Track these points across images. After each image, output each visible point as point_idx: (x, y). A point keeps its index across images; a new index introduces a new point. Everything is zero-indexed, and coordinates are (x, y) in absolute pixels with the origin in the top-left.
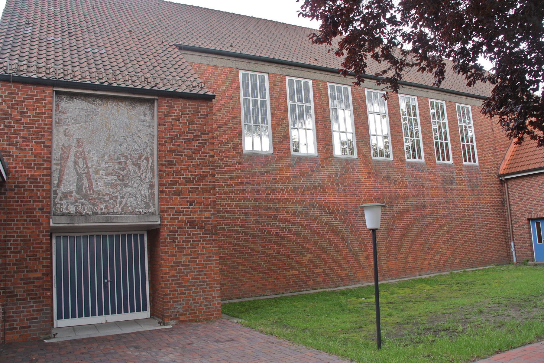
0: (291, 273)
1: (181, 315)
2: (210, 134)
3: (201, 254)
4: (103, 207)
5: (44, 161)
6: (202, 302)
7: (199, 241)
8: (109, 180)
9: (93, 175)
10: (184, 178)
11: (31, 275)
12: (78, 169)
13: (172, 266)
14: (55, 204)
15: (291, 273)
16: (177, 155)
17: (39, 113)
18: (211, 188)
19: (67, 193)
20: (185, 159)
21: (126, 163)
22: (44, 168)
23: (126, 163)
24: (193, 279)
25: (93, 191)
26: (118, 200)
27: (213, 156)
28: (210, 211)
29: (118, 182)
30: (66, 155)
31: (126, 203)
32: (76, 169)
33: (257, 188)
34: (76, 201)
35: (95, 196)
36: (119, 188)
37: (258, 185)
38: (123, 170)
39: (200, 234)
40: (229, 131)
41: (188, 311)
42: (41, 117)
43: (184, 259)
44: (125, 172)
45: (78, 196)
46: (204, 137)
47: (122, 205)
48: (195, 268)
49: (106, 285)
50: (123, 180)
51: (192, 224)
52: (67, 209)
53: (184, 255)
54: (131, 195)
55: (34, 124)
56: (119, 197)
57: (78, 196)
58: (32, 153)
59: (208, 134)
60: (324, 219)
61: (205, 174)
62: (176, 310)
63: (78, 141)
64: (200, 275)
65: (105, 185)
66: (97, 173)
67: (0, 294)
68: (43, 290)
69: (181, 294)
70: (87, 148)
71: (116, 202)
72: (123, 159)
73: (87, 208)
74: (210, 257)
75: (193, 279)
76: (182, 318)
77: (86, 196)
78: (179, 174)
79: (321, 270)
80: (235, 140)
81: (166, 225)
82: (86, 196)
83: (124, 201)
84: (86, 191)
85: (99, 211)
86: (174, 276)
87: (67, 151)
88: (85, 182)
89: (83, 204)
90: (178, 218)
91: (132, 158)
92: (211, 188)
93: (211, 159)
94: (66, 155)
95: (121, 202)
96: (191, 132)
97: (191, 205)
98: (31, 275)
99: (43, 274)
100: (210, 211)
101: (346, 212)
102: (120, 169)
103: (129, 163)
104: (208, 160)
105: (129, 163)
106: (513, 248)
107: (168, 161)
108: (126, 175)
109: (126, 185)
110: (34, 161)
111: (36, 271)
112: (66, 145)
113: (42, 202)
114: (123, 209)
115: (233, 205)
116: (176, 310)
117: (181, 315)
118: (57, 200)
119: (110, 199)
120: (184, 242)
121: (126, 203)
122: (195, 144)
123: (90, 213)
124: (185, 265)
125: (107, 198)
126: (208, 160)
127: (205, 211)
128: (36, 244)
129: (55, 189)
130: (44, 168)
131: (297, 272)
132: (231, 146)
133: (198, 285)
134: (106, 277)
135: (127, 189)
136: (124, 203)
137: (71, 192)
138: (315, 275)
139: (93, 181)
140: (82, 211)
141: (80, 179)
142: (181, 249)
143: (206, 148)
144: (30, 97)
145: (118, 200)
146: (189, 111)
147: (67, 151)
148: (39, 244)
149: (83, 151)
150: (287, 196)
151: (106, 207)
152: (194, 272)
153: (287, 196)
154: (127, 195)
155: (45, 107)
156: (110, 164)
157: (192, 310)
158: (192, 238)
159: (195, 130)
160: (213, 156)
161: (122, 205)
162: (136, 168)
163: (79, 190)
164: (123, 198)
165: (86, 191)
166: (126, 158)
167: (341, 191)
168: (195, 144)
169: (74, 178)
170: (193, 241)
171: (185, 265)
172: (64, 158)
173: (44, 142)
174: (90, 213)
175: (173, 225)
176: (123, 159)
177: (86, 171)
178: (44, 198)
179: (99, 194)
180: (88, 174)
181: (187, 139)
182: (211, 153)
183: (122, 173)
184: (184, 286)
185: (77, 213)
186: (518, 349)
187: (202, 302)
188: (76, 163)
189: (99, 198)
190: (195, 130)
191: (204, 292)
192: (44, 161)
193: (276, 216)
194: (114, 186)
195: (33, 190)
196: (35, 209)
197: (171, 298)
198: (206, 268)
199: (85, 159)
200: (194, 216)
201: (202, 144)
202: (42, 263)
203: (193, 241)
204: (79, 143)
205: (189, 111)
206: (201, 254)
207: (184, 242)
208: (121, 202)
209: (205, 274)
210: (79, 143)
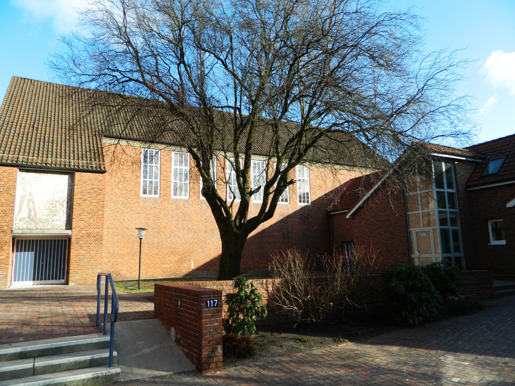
0: (165, 266)
1: (78, 280)
2: (103, 190)
3: (93, 250)
4: (41, 225)
5: (11, 203)
6: (91, 274)
7: (92, 243)
8: (46, 212)
10: (87, 212)
12: (29, 206)
13: (76, 256)
14: (15, 224)
15: (165, 266)
16: (84, 201)
17: (9, 180)
18: (101, 218)
19: (22, 218)
20: (88, 203)
21: (56, 204)
22: (10, 206)
23: (56, 204)
24: (87, 262)
25: (37, 218)
26: (50, 222)
27: (104, 201)
28: (100, 229)
29: (51, 213)
30: (23, 200)
31: (54, 224)
32: (28, 207)
33: (148, 216)
34: (27, 222)
35: (37, 220)
36: (51, 216)
37: (149, 214)
38: (54, 207)
39: (93, 240)
40: (132, 184)
41: (82, 278)
42: (10, 182)
43: (83, 252)
44: (55, 209)
45: (28, 220)
46: (99, 191)
47: (52, 225)
48: (89, 257)
49: (42, 265)
50: (53, 212)
51: (89, 235)
52: (22, 226)
53: (83, 250)
54: (57, 220)
55: (6, 185)
56: (51, 221)
57: (28, 220)
58: (5, 199)
59: (102, 190)
60: (191, 235)
61: (98, 210)
62: (76, 277)
63: (30, 193)
64: (91, 260)
65: (43, 215)
68: (5, 265)
69: (80, 269)
71: (49, 223)
72: (54, 202)
73: (33, 226)
74: (98, 252)
75: (87, 262)
76: (79, 282)
77: (33, 220)
79: (186, 265)
80: (136, 189)
81: (74, 235)
82: (33, 220)
83: (53, 223)
84: (33, 217)
85: (39, 228)
86: (76, 261)
87: (24, 198)
88: (33, 213)
89: (30, 224)
90: (81, 232)
91: (59, 202)
92: (101, 218)
93: (103, 203)
94: (23, 200)
95: (51, 223)
96: (92, 189)
97: (89, 225)
99: (6, 257)
100: (100, 229)
101: (206, 232)
102: (52, 207)
103: (58, 204)
104: (101, 203)
105: (58, 204)
107: (79, 204)
108: (55, 210)
109: (55, 215)
110: (5, 203)
111: (2, 255)
112: (23, 195)
113: (8, 222)
114: (52, 227)
115: (132, 225)
116: (76, 277)
117: (78, 280)
118: (17, 222)
119: (46, 222)
120: (83, 244)
121: (54, 224)
123: (34, 228)
124: (83, 255)
125: (44, 221)
126: (101, 203)
127: (97, 229)
128: (4, 243)
129: (16, 216)
130: (10, 206)
131: (169, 266)
132: (133, 192)
133: (89, 266)
134: (43, 261)
135: (55, 217)
136: (53, 224)
137: (25, 218)
138: (182, 268)
139: (37, 213)
140: (30, 227)
141: (30, 211)
142: (81, 247)
143: (100, 197)
144: (4, 172)
145: (50, 222)
146: (92, 178)
147: (24, 198)
148: (5, 243)
149: (33, 198)
150: (166, 221)
151: (43, 226)
152: (87, 259)
153: (166, 221)
154: (55, 220)
155: (13, 177)
156: (47, 205)
157: (85, 278)
158: (88, 242)
159: (95, 188)
160: (104, 201)
161: (52, 225)
162: (61, 207)
163: (29, 216)
164: (53, 221)
165: (33, 217)
166: (56, 201)
167: (203, 219)
169: (27, 211)
170: (89, 243)
171: (83, 255)
172: (22, 201)
173: (11, 194)
174: (34, 228)
175: (78, 235)
176: (54, 202)
177: (34, 208)
178: (9, 221)
179: (40, 219)
180: (35, 209)
181: (90, 193)
182: (103, 200)
183: (53, 209)
184: (81, 266)
185: (27, 228)
187: (91, 274)
188: (28, 204)
189: (39, 221)
190: (95, 188)
191: (92, 269)
192: (11, 203)
193: (158, 233)
194: (48, 215)
195: (4, 217)
196: (4, 226)
197: (74, 271)
198: (94, 257)
199: (33, 202)
200: (90, 231)
201: (99, 195)
202: (6, 252)
203: (89, 243)
204: (31, 194)
205: (92, 178)
206: (93, 250)
207: (83, 244)
208: (51, 223)
209: (94, 260)
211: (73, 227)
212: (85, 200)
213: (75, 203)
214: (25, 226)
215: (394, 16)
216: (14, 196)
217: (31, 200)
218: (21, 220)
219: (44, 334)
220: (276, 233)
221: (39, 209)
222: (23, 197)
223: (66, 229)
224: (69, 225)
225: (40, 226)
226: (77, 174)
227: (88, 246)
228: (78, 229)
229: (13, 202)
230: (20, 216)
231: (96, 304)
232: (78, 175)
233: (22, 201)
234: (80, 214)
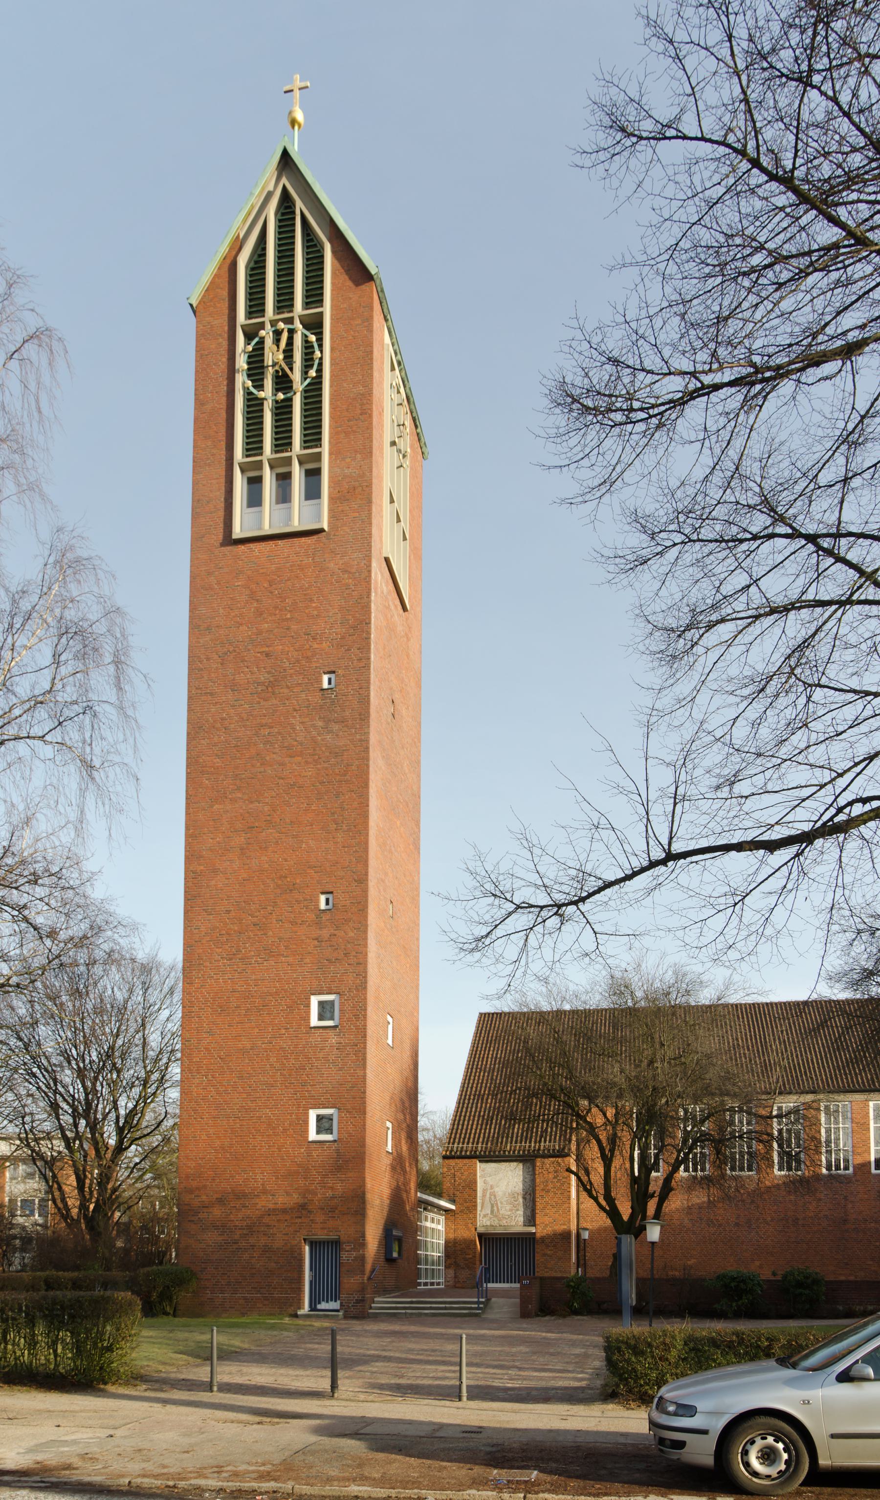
9: (499, 1204)
11: (468, 1256)
43: (549, 1252)
66: (501, 1203)
67: (877, 1109)
70: (496, 1189)
73: (496, 1223)
78: (547, 1203)
82: (496, 1216)
88: (495, 1208)
98: (468, 1256)
101: (737, 1224)
106: (521, 1333)
122: (558, 1184)
141: (492, 1206)
144: (465, 1165)
168: (558, 1184)
186: (377, 1404)
188: (490, 1198)
194: (511, 1210)
199: (495, 1196)
210: (492, 1187)
211: (537, 1222)
212: (548, 1191)
213: (537, 1195)
214: (488, 1224)
215: (800, 881)
216: (475, 1191)
217: (493, 1194)
218: (485, 1216)
219: (172, 1385)
220: (872, 1225)
221: (501, 1203)
222: (484, 1191)
223: (525, 1225)
224: (531, 1219)
225: (504, 1222)
226: (538, 1161)
227: (554, 1246)
228: (542, 1226)
229: (475, 1197)
230: (483, 1213)
231: (209, 1369)
232: (538, 1161)
233: (484, 1196)
234: (544, 1208)
